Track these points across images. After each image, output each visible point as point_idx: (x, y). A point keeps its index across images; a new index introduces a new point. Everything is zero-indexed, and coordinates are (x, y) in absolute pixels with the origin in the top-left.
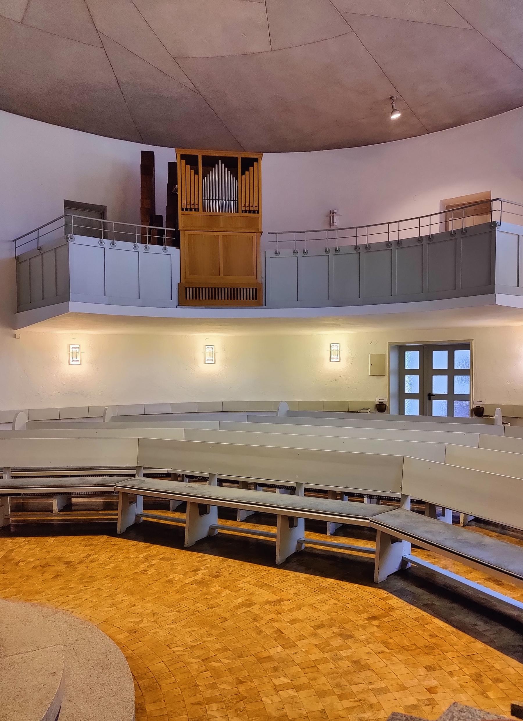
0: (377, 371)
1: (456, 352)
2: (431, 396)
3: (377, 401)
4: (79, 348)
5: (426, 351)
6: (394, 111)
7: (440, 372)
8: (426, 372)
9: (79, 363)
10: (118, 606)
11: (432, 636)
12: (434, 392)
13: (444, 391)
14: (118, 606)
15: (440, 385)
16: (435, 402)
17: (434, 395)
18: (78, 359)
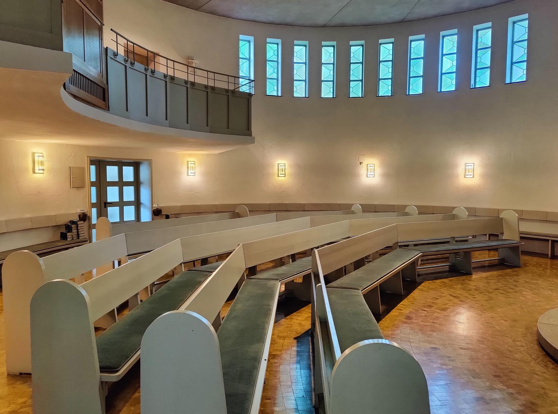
0: (77, 181)
2: (107, 204)
3: (79, 211)
5: (101, 165)
7: (113, 184)
8: (101, 184)
11: (436, 353)
12: (108, 201)
15: (112, 194)
16: (110, 209)
17: (111, 203)
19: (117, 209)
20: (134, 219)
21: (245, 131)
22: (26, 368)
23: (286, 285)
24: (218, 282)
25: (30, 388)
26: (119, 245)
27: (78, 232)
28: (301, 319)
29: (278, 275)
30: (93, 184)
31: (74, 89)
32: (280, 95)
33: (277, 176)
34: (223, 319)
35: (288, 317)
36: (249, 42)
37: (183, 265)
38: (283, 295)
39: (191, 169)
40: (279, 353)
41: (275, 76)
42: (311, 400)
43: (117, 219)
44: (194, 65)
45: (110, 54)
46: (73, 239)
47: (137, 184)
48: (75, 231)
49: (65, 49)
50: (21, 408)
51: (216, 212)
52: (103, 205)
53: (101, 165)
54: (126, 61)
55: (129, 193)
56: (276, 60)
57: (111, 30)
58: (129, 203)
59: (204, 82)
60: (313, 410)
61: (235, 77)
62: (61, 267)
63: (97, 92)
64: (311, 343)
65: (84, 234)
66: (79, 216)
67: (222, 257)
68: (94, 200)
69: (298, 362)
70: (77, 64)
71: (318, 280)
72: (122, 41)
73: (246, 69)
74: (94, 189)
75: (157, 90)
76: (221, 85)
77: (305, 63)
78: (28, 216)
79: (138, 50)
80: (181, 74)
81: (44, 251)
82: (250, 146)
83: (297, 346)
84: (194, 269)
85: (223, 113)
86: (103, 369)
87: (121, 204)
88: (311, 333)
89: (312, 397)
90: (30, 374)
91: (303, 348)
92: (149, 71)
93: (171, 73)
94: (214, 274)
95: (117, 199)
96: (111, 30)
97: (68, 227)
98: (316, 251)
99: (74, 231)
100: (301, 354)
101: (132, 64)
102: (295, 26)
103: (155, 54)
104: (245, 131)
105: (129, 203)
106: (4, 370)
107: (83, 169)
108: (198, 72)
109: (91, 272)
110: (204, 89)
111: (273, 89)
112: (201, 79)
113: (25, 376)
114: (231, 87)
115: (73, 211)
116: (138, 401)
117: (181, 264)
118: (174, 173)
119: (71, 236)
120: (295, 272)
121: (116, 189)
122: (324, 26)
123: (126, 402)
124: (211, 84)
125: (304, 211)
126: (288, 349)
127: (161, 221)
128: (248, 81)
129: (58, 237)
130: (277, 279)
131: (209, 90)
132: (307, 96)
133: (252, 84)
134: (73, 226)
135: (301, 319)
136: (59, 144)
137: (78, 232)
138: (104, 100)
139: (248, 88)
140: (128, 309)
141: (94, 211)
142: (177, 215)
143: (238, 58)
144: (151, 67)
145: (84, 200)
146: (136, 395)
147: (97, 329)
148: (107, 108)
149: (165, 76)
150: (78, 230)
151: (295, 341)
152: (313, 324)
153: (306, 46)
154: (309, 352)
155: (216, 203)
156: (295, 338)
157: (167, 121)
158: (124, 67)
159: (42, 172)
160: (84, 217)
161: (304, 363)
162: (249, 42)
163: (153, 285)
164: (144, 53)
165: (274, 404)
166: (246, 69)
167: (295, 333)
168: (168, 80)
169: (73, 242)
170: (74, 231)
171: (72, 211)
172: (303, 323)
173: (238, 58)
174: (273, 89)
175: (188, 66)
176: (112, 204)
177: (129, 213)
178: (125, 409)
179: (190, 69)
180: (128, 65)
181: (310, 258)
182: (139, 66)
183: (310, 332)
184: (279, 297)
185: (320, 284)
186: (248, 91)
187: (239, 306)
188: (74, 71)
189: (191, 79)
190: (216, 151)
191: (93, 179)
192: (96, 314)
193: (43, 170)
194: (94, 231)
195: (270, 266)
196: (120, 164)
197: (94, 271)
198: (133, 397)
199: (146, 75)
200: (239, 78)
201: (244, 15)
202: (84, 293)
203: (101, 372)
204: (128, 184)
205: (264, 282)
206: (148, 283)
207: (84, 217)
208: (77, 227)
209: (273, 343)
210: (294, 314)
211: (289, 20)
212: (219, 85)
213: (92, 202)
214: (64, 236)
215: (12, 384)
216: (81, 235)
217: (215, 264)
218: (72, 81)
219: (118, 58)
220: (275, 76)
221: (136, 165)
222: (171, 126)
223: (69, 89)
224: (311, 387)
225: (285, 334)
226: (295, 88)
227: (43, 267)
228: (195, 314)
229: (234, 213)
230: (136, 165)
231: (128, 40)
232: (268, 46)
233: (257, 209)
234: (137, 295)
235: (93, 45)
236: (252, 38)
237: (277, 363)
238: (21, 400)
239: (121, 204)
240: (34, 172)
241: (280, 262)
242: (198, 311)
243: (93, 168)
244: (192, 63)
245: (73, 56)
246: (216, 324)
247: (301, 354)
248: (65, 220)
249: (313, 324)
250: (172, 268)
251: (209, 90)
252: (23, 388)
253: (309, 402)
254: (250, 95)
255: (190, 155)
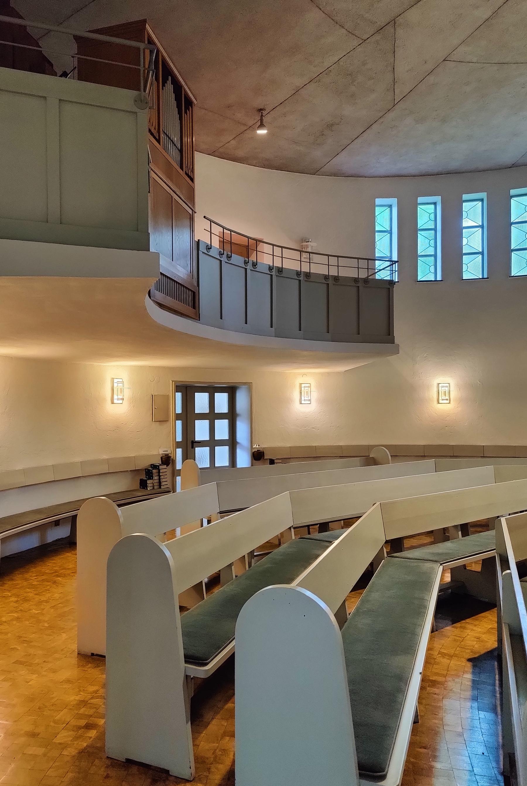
0: (160, 414)
1: (216, 395)
2: (195, 444)
3: (161, 452)
4: (310, 387)
5: (188, 391)
6: (262, 126)
7: (202, 417)
8: (188, 416)
9: (309, 402)
10: (48, 755)
13: (206, 437)
14: (48, 755)
16: (198, 450)
18: (447, 398)
19: (206, 450)
20: (227, 465)
21: (382, 336)
22: (100, 648)
23: (453, 571)
24: (345, 556)
25: (102, 674)
26: (208, 497)
27: (160, 479)
28: (479, 630)
29: (439, 554)
30: (178, 417)
31: (159, 296)
32: (439, 278)
33: (436, 402)
34: (349, 614)
35: (458, 625)
36: (390, 206)
37: (292, 529)
38: (448, 589)
39: (306, 393)
40: (440, 679)
41: (431, 251)
42: (498, 762)
43: (206, 464)
44: (309, 250)
45: (202, 248)
46: (153, 489)
47: (232, 416)
48: (156, 478)
49: (152, 249)
50: (92, 698)
51: (341, 457)
52: (189, 444)
53: (188, 391)
54: (221, 254)
55: (222, 429)
56: (433, 227)
57: (205, 217)
58: (221, 443)
59: (322, 270)
60: (501, 778)
61: (368, 259)
62: (142, 519)
63: (185, 298)
64: (497, 672)
65: (166, 483)
66: (162, 458)
67: (348, 522)
68: (179, 438)
69: (474, 699)
70: (165, 265)
71: (505, 564)
72: (217, 230)
73: (385, 246)
74: (179, 423)
75: (260, 287)
76: (348, 272)
77: (482, 227)
78: (105, 457)
79: (236, 239)
80: (292, 265)
81: (123, 500)
82: (392, 359)
83: (473, 673)
84: (308, 536)
85: (352, 313)
86: (189, 659)
87: (212, 443)
88: (496, 655)
89: (498, 756)
90: (104, 657)
91: (484, 677)
92: (251, 262)
93: (278, 263)
94: (336, 542)
95: (207, 438)
96: (205, 217)
97: (150, 472)
98: (503, 520)
99: (156, 478)
100: (479, 687)
101: (229, 257)
102: (463, 172)
103: (258, 241)
104: (382, 336)
105: (221, 443)
106: (74, 647)
107: (167, 397)
108: (316, 258)
109: (174, 530)
110: (324, 281)
111: (427, 271)
112: (319, 268)
113: (96, 659)
114: (363, 275)
115: (155, 453)
116: (231, 715)
117: (290, 528)
118: (281, 400)
119: (151, 485)
120: (469, 552)
121: (206, 423)
122: (514, 166)
123: (216, 713)
124: (333, 272)
125: (484, 457)
126: (458, 676)
127: (264, 468)
128: (388, 263)
129: (137, 485)
130: (436, 561)
131: (330, 282)
132: (485, 276)
133: (396, 267)
134: (154, 471)
135: (479, 630)
136: (141, 367)
137: (160, 479)
138: (194, 307)
139: (389, 273)
140: (220, 586)
141: (179, 451)
142: (285, 460)
143: (373, 231)
144: (253, 258)
145: (162, 441)
146: (229, 705)
147: (182, 609)
148: (197, 317)
149: (271, 268)
150: (159, 476)
151: (469, 664)
152: (500, 641)
153: (482, 200)
154: (494, 685)
155: (341, 444)
156: (469, 660)
157: (273, 329)
158: (218, 262)
159: (121, 401)
160: (167, 460)
161: (487, 700)
162: (390, 206)
163: (251, 554)
164: (244, 241)
165: (435, 757)
166: (385, 246)
167: (468, 651)
168: (273, 274)
169: (153, 492)
170: (156, 478)
171: (153, 453)
172: (484, 637)
173: (374, 232)
174: (427, 271)
175: (301, 252)
176: (202, 444)
177: (222, 456)
178: (214, 722)
179: (304, 255)
180: (224, 259)
181: (492, 533)
182: (237, 259)
183: (496, 654)
184: (440, 591)
185: (508, 571)
186: (388, 278)
187: (375, 595)
188: (161, 273)
189: (305, 268)
190: (341, 368)
191: (179, 410)
192: (181, 585)
193: (123, 399)
194: (179, 479)
195: (425, 542)
196: (212, 390)
197: (178, 531)
198: (226, 707)
199: (246, 269)
200: (375, 260)
201: (382, 171)
202: (168, 553)
203: (186, 662)
204: (221, 416)
205: (414, 564)
206: (245, 551)
207: (167, 460)
208: (159, 472)
209: (428, 661)
210: (468, 620)
211: (454, 165)
212: (344, 273)
213: (177, 441)
214: (143, 484)
215: (83, 666)
216: (163, 484)
217: (337, 532)
218: (158, 288)
219: (212, 252)
220: (431, 251)
221: (231, 391)
222: (278, 335)
223: (154, 297)
224: (498, 742)
225: (452, 652)
226: (464, 266)
227: (122, 520)
228: (308, 593)
229: (368, 458)
230: (231, 391)
231: (224, 228)
232: (420, 208)
233: (402, 454)
234: (230, 566)
235: (182, 240)
236: (394, 201)
237: (438, 695)
238: (92, 689)
239: (212, 443)
240: (113, 403)
241: (442, 535)
242: (316, 594)
243: (179, 395)
244: (307, 246)
245: (161, 255)
246: (341, 616)
247: (479, 687)
248: (144, 464)
249: (500, 641)
250: (277, 532)
251: (330, 282)
252: (93, 672)
253: (494, 765)
254: (391, 283)
255: (304, 374)
